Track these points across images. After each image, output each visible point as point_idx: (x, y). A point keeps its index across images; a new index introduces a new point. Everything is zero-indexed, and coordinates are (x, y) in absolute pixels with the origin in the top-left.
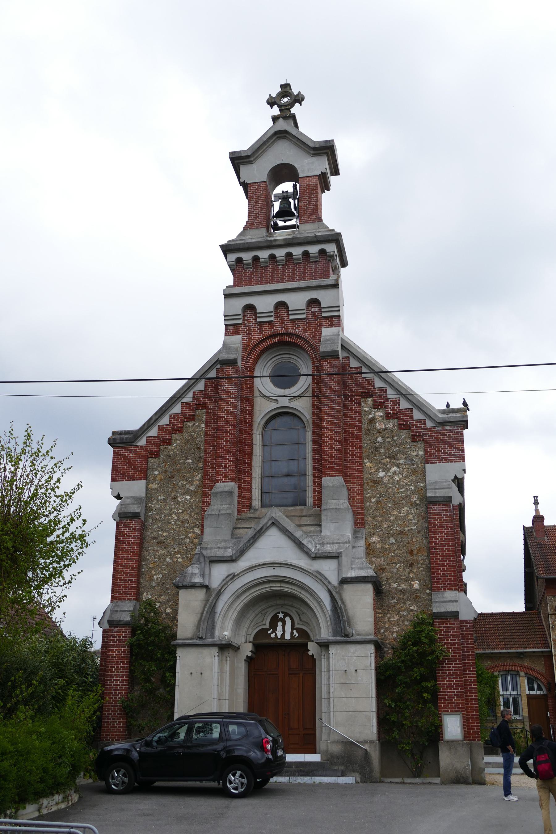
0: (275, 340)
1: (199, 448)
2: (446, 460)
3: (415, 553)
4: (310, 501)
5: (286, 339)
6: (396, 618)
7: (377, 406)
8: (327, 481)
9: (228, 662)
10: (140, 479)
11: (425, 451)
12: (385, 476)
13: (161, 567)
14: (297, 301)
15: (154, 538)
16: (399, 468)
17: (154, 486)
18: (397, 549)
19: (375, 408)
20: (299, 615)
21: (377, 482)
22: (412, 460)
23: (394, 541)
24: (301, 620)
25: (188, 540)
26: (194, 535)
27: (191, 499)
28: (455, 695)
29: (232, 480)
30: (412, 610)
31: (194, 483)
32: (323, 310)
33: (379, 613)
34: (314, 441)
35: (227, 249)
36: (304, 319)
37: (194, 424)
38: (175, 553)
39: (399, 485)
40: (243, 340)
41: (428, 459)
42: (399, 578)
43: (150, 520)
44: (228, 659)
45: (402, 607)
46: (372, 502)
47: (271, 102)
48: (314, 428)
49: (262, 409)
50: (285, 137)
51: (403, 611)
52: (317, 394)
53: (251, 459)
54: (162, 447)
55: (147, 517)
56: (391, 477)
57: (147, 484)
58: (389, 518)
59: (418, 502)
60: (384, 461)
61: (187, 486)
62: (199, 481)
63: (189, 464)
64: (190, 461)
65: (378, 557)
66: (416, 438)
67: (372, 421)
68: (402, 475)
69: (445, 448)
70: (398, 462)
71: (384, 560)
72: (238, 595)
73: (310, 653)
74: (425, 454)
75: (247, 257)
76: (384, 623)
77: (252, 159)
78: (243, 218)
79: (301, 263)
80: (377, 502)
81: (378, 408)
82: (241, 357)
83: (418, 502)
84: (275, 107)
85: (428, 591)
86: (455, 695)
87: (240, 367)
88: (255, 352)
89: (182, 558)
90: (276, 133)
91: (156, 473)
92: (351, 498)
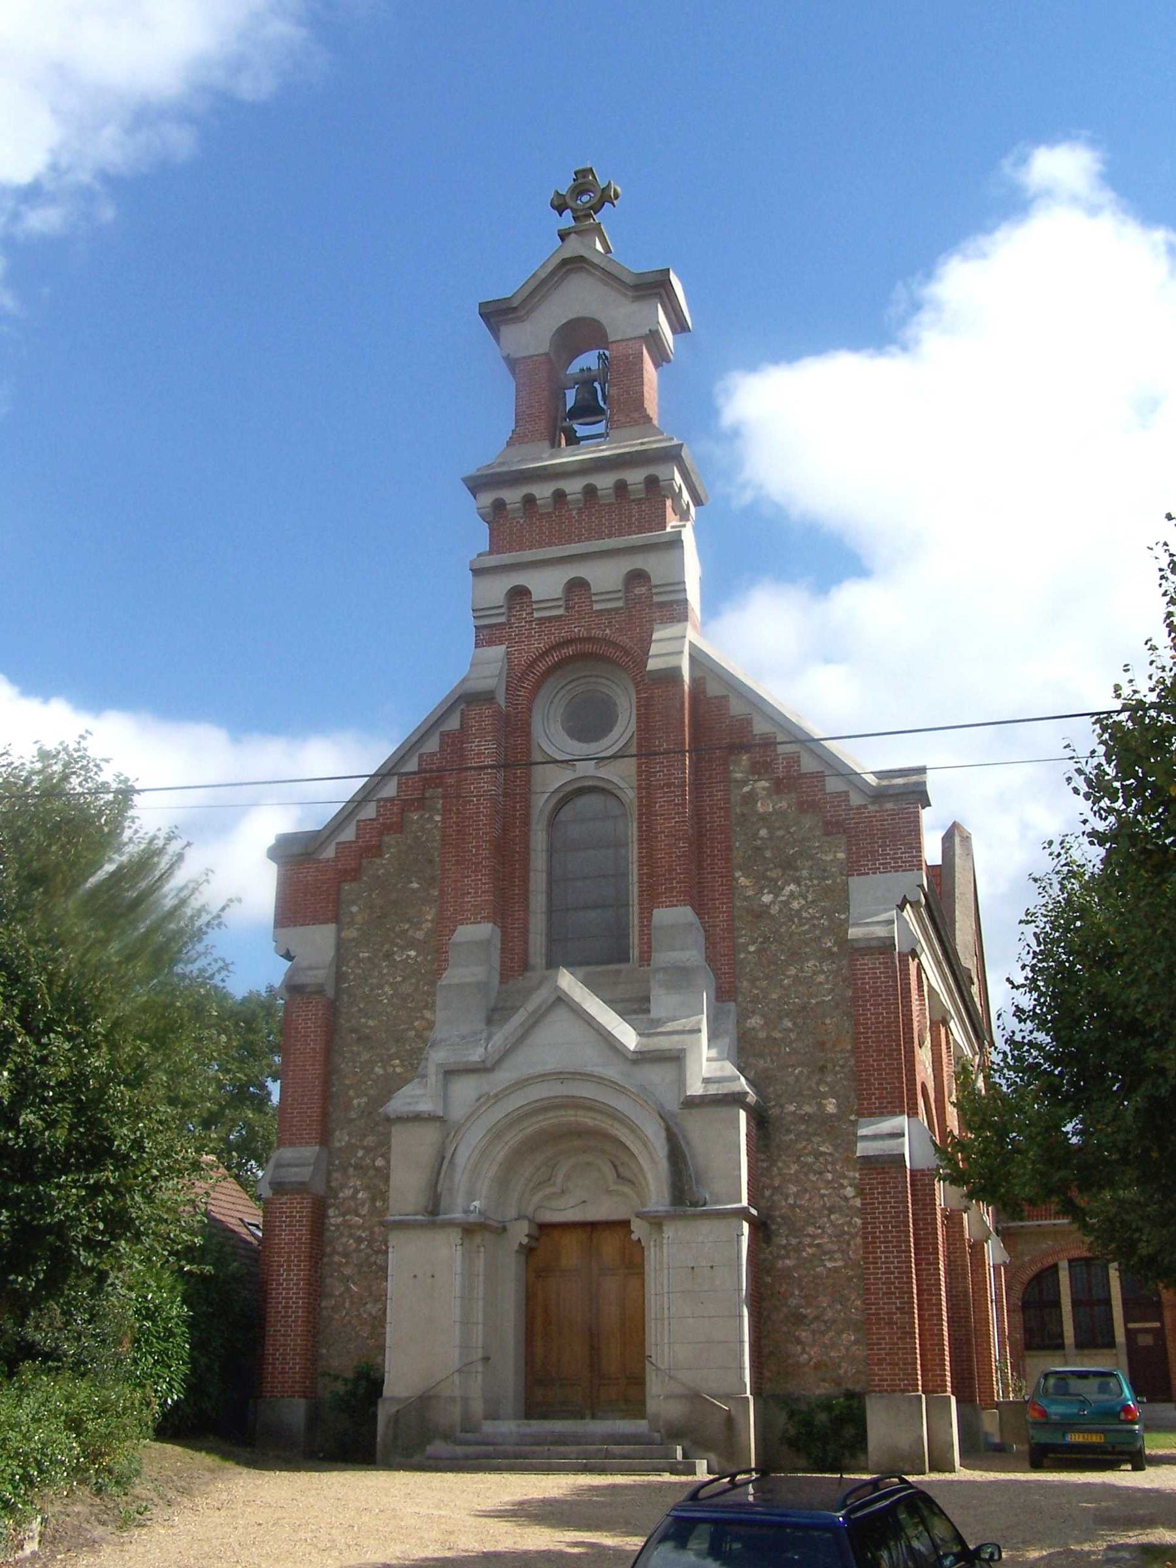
0: (570, 651)
1: (431, 861)
2: (886, 868)
3: (828, 1045)
4: (635, 953)
5: (588, 648)
6: (794, 1168)
7: (760, 768)
8: (664, 915)
9: (482, 1255)
10: (325, 922)
11: (849, 851)
12: (773, 902)
13: (365, 1083)
14: (605, 577)
15: (353, 1031)
16: (799, 885)
17: (350, 933)
18: (796, 1040)
19: (753, 774)
20: (615, 1167)
21: (761, 913)
22: (825, 871)
23: (790, 1025)
24: (619, 1176)
25: (412, 1033)
26: (424, 1023)
27: (416, 956)
28: (897, 1308)
29: (486, 919)
30: (822, 1154)
31: (424, 926)
32: (654, 591)
33: (763, 1161)
34: (641, 840)
35: (476, 485)
36: (621, 608)
37: (422, 816)
38: (391, 1058)
39: (800, 918)
40: (508, 653)
41: (853, 867)
42: (800, 1093)
43: (345, 998)
44: (482, 1249)
45: (805, 1148)
46: (750, 953)
47: (560, 206)
48: (640, 815)
49: (550, 781)
50: (581, 269)
51: (807, 1155)
52: (645, 749)
53: (525, 880)
54: (364, 861)
55: (338, 991)
56: (786, 903)
57: (339, 931)
58: (782, 980)
59: (835, 949)
60: (772, 874)
61: (410, 933)
62: (432, 921)
63: (414, 891)
64: (415, 885)
65: (761, 1055)
66: (832, 827)
67: (751, 798)
68: (805, 898)
69: (884, 846)
70: (798, 874)
71: (772, 1061)
72: (496, 1134)
73: (634, 1237)
74: (848, 858)
75: (513, 496)
76: (772, 1179)
77: (522, 313)
78: (507, 425)
79: (612, 504)
80: (759, 951)
81: (759, 774)
82: (504, 687)
83: (835, 949)
84: (568, 213)
85: (852, 1118)
86: (897, 1308)
87: (503, 704)
88: (527, 679)
89: (403, 1066)
90: (565, 262)
91: (354, 909)
92: (711, 944)
